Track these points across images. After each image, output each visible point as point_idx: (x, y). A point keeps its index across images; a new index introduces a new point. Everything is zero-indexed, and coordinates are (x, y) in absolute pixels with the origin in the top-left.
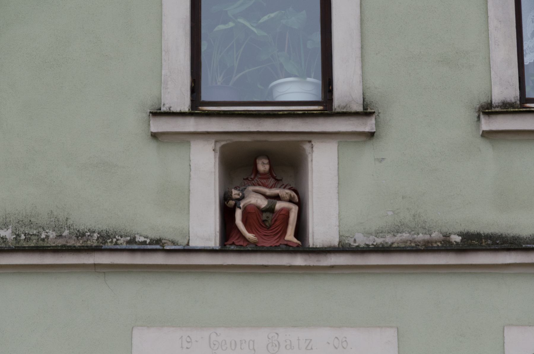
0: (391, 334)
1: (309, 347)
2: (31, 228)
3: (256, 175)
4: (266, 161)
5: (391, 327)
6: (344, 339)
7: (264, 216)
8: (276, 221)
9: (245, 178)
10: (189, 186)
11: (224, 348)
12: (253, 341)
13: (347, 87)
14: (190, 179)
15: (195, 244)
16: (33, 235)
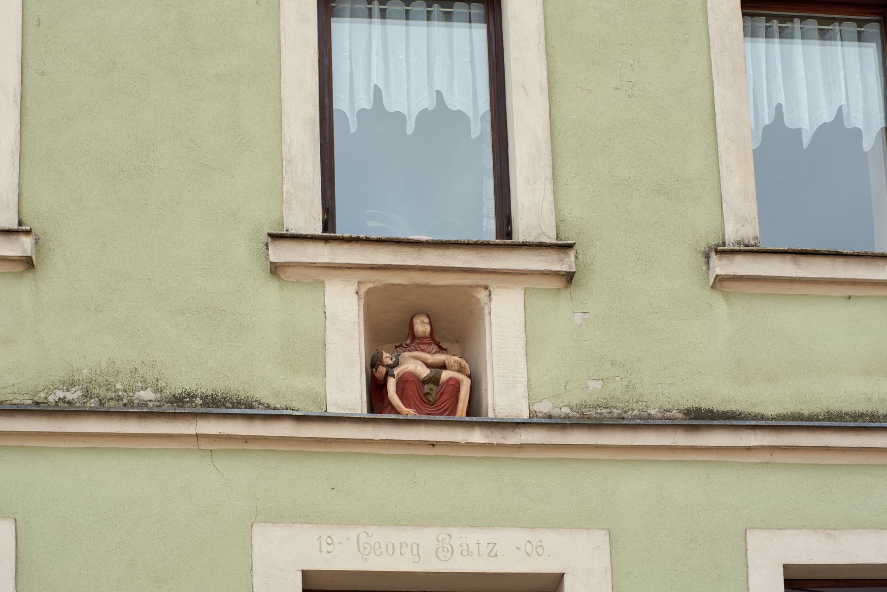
0: (600, 538)
1: (493, 554)
2: (108, 390)
3: (412, 341)
4: (427, 320)
5: (603, 529)
6: (539, 544)
7: (427, 388)
8: (442, 393)
9: (397, 344)
10: (324, 340)
11: (378, 553)
12: (418, 545)
13: (532, 216)
14: (325, 331)
15: (332, 410)
16: (112, 399)
